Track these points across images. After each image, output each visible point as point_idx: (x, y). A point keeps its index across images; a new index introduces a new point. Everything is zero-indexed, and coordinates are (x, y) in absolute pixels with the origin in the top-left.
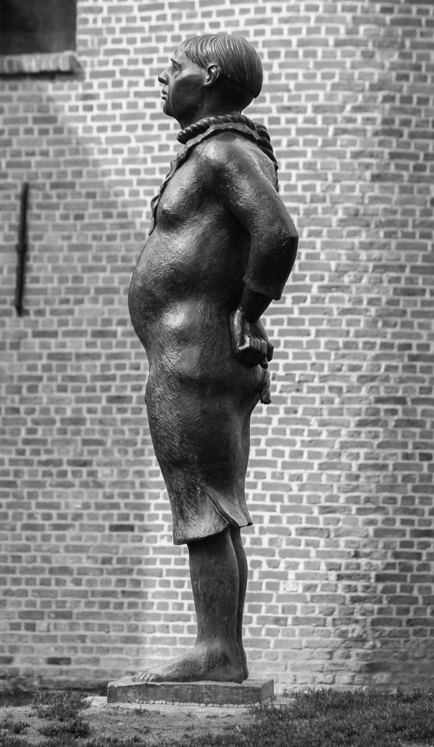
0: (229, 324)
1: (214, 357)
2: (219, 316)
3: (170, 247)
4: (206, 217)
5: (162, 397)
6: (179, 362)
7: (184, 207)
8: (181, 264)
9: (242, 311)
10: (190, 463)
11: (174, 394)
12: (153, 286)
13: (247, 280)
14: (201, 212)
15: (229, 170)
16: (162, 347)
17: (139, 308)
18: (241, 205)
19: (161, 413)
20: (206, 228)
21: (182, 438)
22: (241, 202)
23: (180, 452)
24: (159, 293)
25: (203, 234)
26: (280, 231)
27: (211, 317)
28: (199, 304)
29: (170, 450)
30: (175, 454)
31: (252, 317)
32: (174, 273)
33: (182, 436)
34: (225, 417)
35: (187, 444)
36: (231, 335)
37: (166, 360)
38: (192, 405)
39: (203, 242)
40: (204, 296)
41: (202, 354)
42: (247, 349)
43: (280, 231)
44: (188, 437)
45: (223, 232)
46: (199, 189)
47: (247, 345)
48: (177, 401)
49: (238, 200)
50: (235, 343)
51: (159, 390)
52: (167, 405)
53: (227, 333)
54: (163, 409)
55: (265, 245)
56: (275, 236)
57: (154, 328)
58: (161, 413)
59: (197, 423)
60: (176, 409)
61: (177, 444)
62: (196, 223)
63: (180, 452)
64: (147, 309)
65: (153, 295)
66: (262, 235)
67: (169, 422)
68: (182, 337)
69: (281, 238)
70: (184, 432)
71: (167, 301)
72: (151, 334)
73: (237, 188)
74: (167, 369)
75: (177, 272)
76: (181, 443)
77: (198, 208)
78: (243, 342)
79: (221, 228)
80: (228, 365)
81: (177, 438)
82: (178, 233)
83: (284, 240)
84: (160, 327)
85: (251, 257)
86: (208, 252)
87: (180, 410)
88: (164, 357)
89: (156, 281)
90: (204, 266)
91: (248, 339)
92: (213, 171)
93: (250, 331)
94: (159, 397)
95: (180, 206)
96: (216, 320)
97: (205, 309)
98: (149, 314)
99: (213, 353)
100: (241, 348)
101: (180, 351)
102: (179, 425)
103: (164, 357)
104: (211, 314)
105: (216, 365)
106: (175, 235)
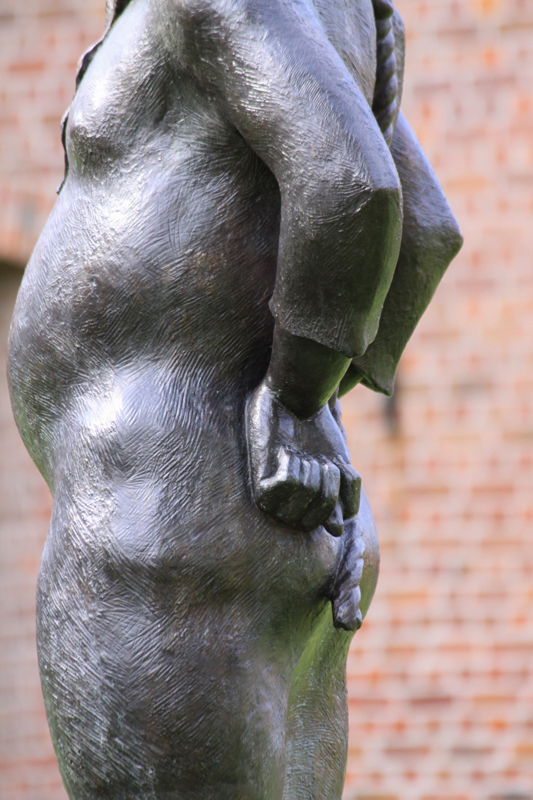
0: (239, 421)
1: (197, 509)
2: (214, 401)
3: (89, 222)
4: (177, 144)
5: (64, 617)
6: (106, 522)
7: (123, 118)
8: (114, 269)
9: (273, 388)
10: (136, 790)
11: (93, 606)
12: (50, 328)
13: (276, 306)
14: (167, 130)
15: (220, 18)
16: (68, 485)
17: (22, 385)
18: (251, 108)
19: (63, 656)
20: (178, 172)
21: (114, 723)
22: (252, 102)
23: (109, 761)
24: (64, 345)
25: (170, 188)
26: (348, 175)
27: (190, 404)
28: (161, 372)
29: (87, 755)
30: (97, 764)
31: (301, 403)
32: (97, 290)
33: (113, 716)
34: (231, 664)
35: (126, 739)
36: (244, 450)
37: (76, 518)
38: (140, 635)
39: (173, 209)
40: (173, 350)
41: (164, 501)
42: (281, 487)
43: (348, 175)
44: (128, 720)
45: (220, 184)
46: (157, 69)
47: (282, 475)
48: (101, 626)
49: (243, 95)
50: (254, 470)
51: (59, 597)
52: (76, 636)
53: (233, 444)
54: (68, 647)
55: (310, 213)
56: (335, 187)
57: (56, 434)
58: (63, 656)
59: (150, 681)
60: (98, 648)
61: (102, 739)
62: (152, 160)
63: (109, 761)
64: (37, 385)
65: (50, 351)
66: (302, 187)
67: (81, 682)
68: (117, 460)
69: (352, 193)
70: (118, 706)
71: (81, 364)
72: (52, 452)
73: (241, 64)
74: (77, 543)
75: (105, 290)
76: (111, 735)
77: (158, 121)
78: (272, 467)
79: (216, 171)
80: (234, 528)
81: (102, 723)
82: (108, 185)
83: (357, 199)
84: (66, 434)
85: (284, 242)
86: (182, 234)
87: (109, 648)
88: (72, 510)
89: (56, 313)
90: (172, 273)
91: (284, 460)
92: (182, 21)
93: (297, 438)
94: (58, 615)
95: (113, 117)
96: (204, 411)
97: (177, 385)
98: (43, 399)
99: (193, 498)
100: (266, 484)
101: (108, 493)
102: (104, 688)
103: (72, 510)
104: (191, 395)
105: (201, 528)
106: (102, 192)
